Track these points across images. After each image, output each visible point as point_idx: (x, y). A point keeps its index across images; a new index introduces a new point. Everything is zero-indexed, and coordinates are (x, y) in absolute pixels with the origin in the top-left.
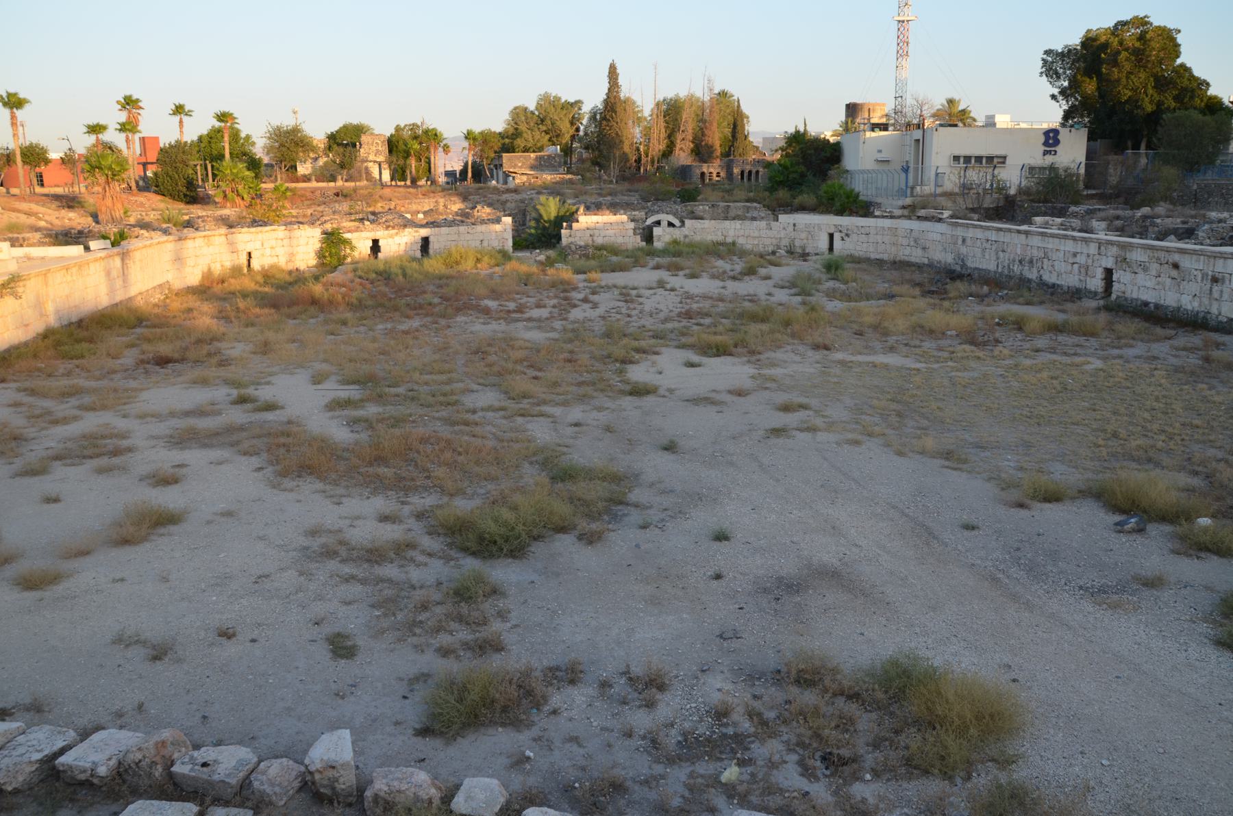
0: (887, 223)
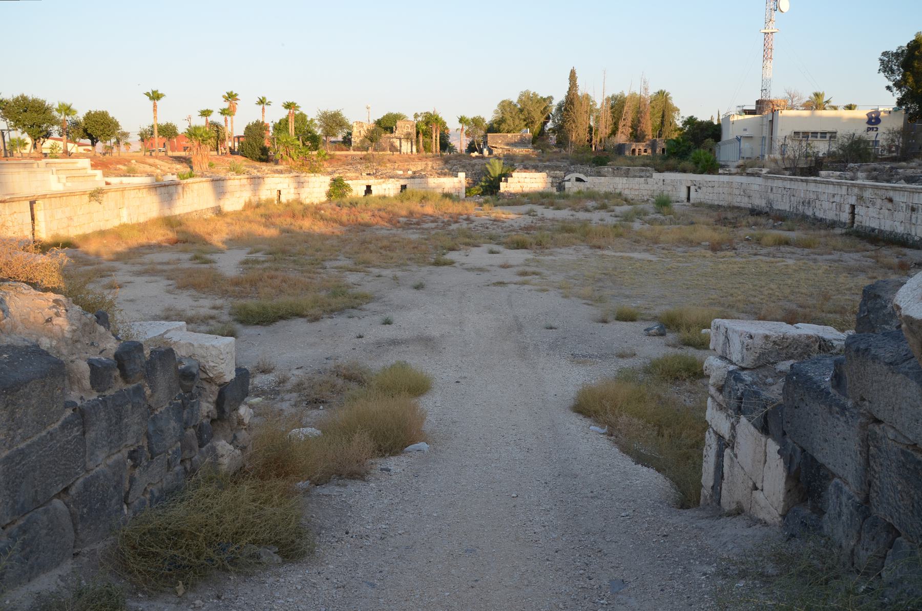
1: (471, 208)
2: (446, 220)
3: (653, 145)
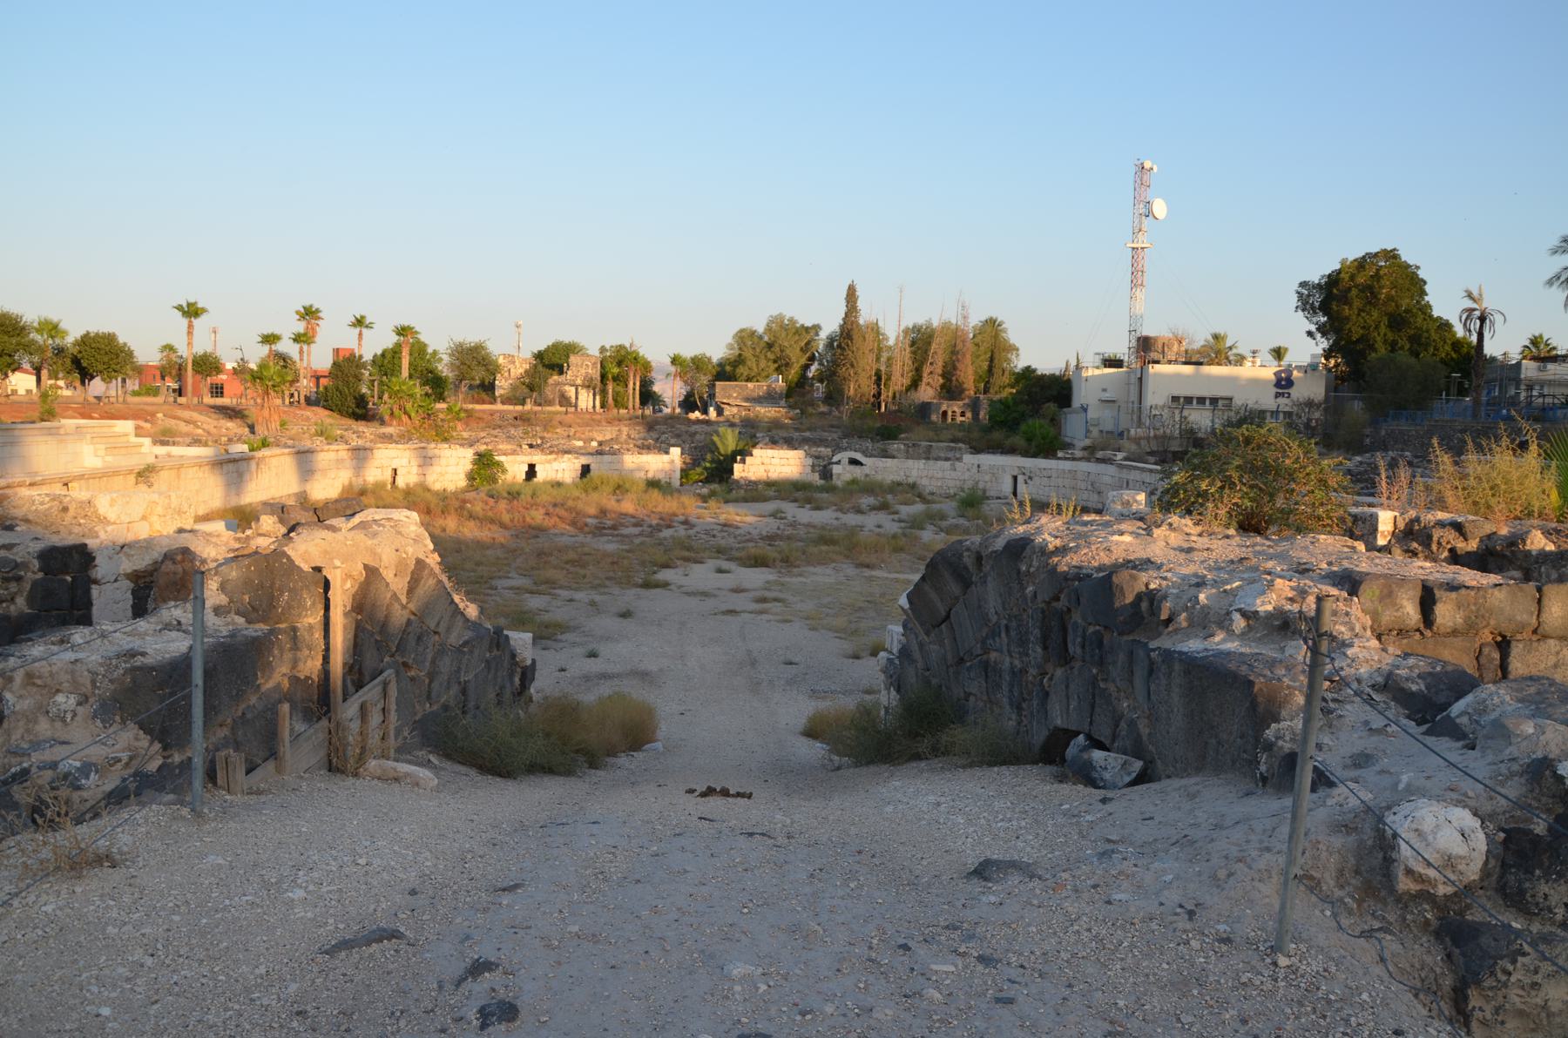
0: (1067, 465)
1: (689, 505)
2: (654, 522)
3: (975, 406)
